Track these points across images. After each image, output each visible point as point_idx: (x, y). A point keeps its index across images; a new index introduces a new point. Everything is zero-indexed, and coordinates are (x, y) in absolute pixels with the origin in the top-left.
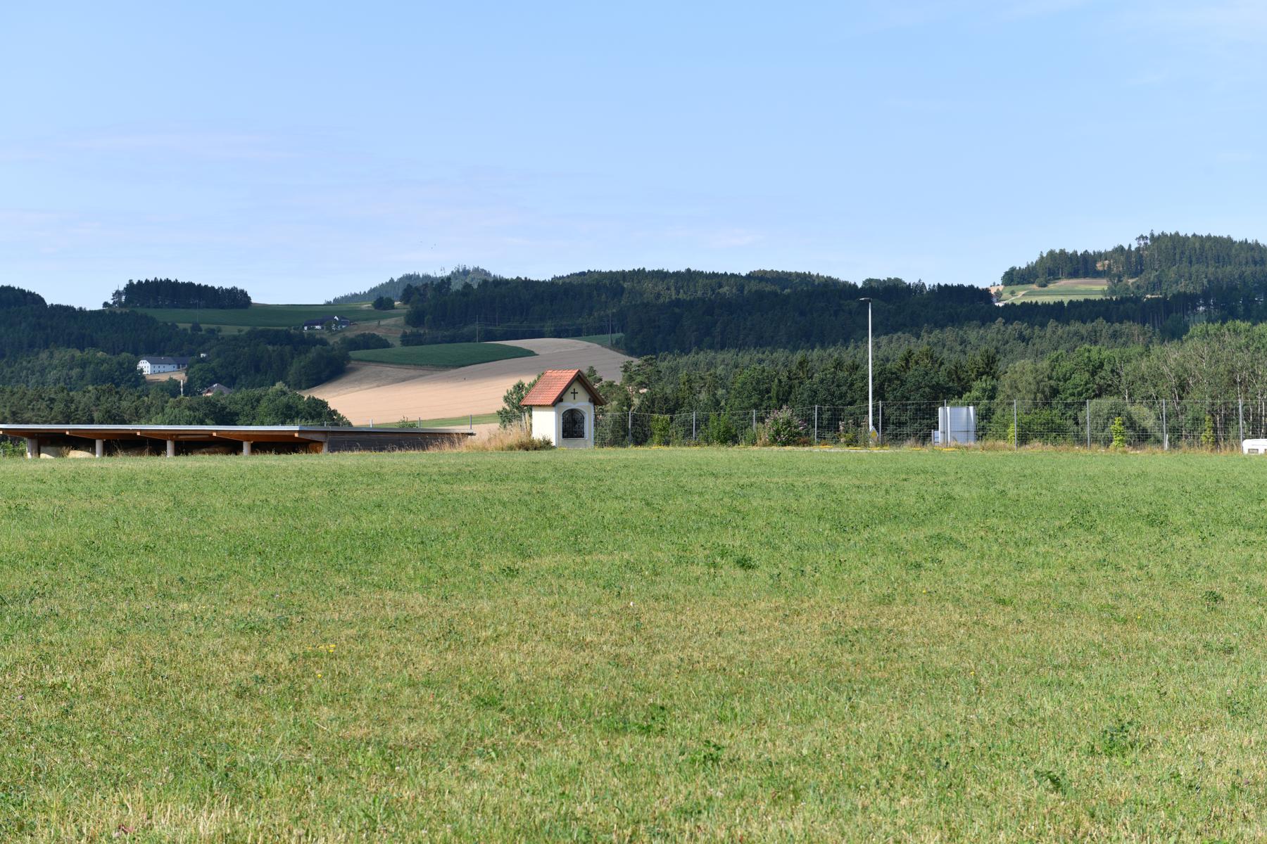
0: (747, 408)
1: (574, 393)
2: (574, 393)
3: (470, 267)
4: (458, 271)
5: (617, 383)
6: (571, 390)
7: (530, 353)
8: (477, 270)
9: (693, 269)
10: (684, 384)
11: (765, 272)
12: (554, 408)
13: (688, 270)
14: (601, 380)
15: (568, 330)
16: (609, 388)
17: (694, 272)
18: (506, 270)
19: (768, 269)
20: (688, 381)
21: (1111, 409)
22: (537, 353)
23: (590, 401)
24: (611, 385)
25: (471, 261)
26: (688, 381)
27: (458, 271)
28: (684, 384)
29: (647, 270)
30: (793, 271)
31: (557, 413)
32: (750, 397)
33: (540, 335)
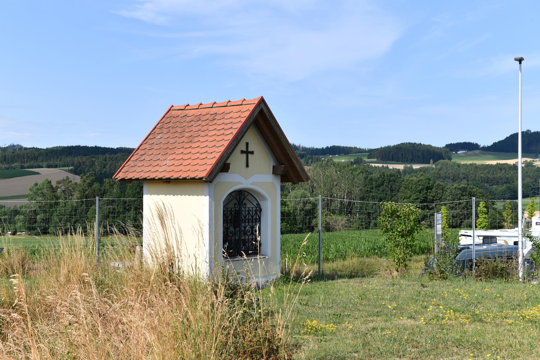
0: (135, 194)
1: (247, 152)
2: (247, 152)
3: (15, 144)
4: (11, 145)
5: (78, 183)
6: (242, 146)
7: (38, 173)
8: (18, 145)
9: (97, 146)
10: (107, 184)
11: (122, 148)
12: (206, 188)
13: (96, 146)
14: (71, 181)
15: (52, 166)
16: (75, 185)
17: (98, 147)
18: (27, 144)
19: (123, 147)
20: (109, 182)
21: (302, 195)
22: (40, 173)
23: (275, 172)
24: (76, 184)
25: (16, 141)
26: (109, 182)
27: (11, 145)
28: (107, 184)
29: (81, 146)
30: (132, 148)
31: (213, 200)
32: (136, 189)
33: (42, 167)
